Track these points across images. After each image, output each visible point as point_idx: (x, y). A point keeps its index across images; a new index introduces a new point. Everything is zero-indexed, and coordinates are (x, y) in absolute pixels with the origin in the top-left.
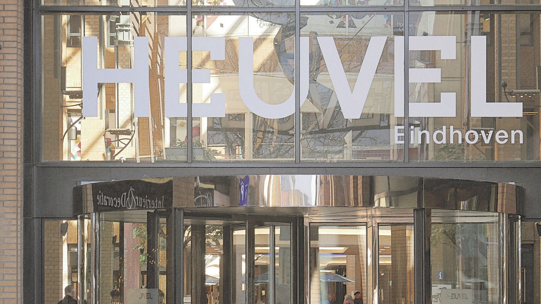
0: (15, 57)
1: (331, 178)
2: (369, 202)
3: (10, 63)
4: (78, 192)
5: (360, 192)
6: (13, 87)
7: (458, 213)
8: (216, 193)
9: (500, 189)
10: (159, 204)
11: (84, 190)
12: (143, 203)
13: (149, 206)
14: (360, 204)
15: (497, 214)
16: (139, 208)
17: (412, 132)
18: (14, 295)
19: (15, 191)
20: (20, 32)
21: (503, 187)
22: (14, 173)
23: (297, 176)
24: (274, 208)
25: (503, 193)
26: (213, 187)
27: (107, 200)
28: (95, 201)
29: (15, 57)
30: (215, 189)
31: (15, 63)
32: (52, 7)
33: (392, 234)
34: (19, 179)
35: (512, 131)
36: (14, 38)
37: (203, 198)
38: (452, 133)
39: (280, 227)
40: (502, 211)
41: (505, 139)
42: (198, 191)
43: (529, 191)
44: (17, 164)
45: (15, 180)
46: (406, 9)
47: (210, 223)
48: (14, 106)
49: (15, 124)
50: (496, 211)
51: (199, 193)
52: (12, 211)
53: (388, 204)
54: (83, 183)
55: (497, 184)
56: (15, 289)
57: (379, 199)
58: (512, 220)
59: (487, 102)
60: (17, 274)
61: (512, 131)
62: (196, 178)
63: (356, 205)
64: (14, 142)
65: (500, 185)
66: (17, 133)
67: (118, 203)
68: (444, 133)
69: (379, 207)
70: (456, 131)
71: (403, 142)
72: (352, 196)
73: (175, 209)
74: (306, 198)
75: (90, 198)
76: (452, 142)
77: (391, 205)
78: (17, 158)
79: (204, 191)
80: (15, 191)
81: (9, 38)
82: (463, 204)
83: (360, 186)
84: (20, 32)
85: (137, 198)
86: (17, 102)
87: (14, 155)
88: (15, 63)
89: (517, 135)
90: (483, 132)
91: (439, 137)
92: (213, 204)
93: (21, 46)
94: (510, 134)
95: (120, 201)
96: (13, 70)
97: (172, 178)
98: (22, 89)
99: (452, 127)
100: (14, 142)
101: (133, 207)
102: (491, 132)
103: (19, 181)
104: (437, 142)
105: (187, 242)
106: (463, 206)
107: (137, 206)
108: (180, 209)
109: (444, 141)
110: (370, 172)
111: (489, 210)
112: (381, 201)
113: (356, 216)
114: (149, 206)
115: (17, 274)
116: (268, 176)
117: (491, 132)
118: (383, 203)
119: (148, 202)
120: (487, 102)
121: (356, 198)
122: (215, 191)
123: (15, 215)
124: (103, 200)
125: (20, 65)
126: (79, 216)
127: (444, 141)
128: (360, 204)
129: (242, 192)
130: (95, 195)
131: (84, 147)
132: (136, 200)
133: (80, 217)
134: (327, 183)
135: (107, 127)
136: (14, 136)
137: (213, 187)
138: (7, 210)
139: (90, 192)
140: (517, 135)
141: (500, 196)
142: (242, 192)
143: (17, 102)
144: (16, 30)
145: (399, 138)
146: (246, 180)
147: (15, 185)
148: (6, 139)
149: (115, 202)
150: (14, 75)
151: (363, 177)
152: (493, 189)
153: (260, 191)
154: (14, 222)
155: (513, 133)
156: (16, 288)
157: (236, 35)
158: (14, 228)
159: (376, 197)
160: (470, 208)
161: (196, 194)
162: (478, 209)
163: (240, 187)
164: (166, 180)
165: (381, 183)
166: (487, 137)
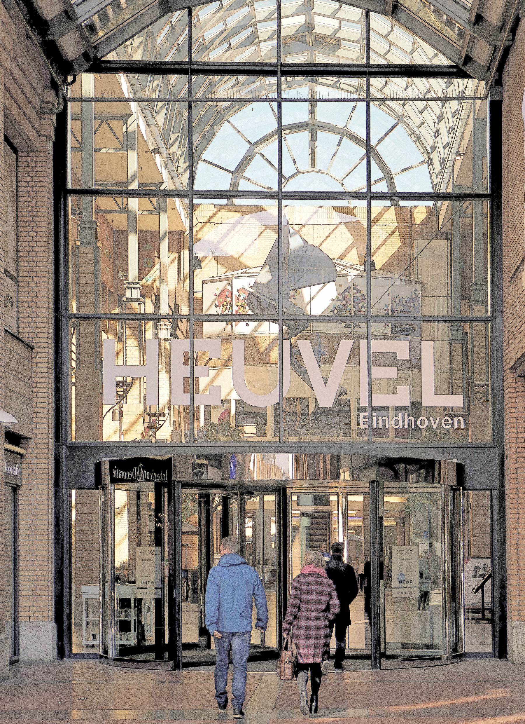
3: (42, 380)
4: (98, 466)
7: (408, 484)
10: (162, 477)
11: (103, 466)
12: (150, 476)
13: (154, 478)
19: (45, 466)
20: (50, 380)
24: (258, 480)
26: (207, 462)
28: (111, 474)
31: (46, 411)
32: (100, 190)
34: (50, 435)
35: (401, 427)
36: (46, 340)
37: (199, 471)
39: (64, 491)
41: (449, 424)
42: (195, 466)
45: (47, 472)
47: (213, 492)
49: (46, 411)
51: (196, 467)
53: (351, 477)
54: (103, 459)
57: (344, 472)
59: (436, 393)
61: (401, 427)
62: (193, 456)
63: (325, 478)
67: (130, 476)
70: (410, 418)
71: (367, 427)
72: (322, 470)
73: (174, 481)
74: (286, 472)
75: (108, 471)
76: (406, 426)
78: (48, 438)
80: (45, 466)
81: (41, 340)
82: (412, 477)
84: (50, 380)
85: (145, 472)
87: (46, 426)
88: (46, 360)
89: (459, 422)
92: (208, 477)
94: (453, 421)
95: (131, 474)
99: (406, 415)
101: (142, 479)
103: (50, 432)
104: (397, 427)
108: (178, 482)
109: (400, 426)
110: (336, 452)
112: (346, 475)
114: (154, 478)
116: (253, 454)
118: (348, 477)
119: (154, 476)
120: (436, 393)
121: (325, 472)
122: (209, 467)
123: (47, 460)
124: (118, 474)
127: (400, 426)
128: (328, 478)
129: (232, 466)
130: (111, 469)
133: (102, 487)
135: (145, 410)
137: (207, 462)
138: (40, 481)
139: (107, 467)
140: (459, 422)
142: (232, 466)
146: (233, 457)
148: (39, 423)
149: (127, 475)
150: (45, 400)
155: (456, 419)
158: (46, 497)
159: (341, 471)
160: (418, 481)
164: (167, 457)
165: (345, 460)
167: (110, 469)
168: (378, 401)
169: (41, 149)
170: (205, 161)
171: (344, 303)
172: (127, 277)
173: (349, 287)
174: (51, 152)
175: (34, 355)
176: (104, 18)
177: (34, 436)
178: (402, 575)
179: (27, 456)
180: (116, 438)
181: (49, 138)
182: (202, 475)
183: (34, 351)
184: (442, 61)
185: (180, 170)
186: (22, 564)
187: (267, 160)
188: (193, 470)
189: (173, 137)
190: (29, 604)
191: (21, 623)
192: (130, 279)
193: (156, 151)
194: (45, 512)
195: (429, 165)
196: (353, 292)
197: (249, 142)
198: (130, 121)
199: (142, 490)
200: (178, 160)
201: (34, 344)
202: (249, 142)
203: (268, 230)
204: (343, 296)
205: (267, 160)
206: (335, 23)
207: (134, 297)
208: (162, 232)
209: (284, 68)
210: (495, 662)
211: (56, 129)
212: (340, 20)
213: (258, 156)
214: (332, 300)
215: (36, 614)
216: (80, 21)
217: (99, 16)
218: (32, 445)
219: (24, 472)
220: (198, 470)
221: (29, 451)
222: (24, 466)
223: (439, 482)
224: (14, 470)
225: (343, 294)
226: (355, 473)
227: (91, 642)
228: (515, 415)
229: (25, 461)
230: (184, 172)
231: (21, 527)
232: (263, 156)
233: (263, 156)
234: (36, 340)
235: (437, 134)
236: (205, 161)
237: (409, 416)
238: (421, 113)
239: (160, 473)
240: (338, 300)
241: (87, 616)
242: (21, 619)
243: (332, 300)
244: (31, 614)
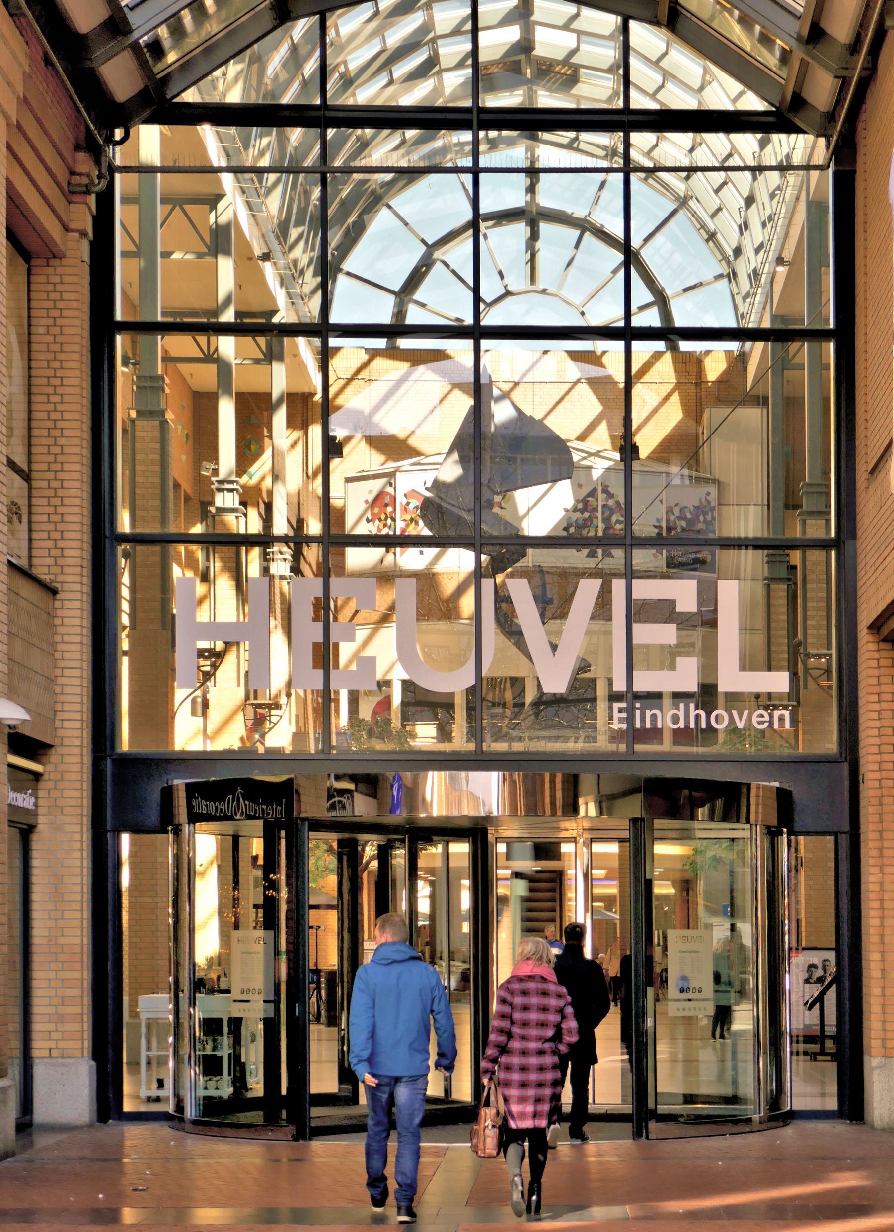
0: (78, 604)
1: (518, 776)
2: (572, 809)
5: (559, 794)
6: (77, 647)
8: (357, 796)
9: (753, 792)
10: (277, 811)
11: (175, 792)
12: (256, 810)
14: (559, 813)
15: (749, 826)
16: (249, 817)
17: (638, 712)
18: (77, 940)
20: (85, 518)
21: (758, 787)
22: (78, 733)
23: (472, 774)
24: (438, 819)
25: (758, 796)
26: (352, 786)
27: (206, 806)
28: (190, 807)
29: (78, 690)
30: (356, 790)
33: (620, 851)
37: (340, 802)
38: (693, 713)
40: (757, 821)
42: (332, 793)
43: (799, 795)
44: (82, 755)
46: (628, 542)
47: (362, 837)
48: (77, 673)
50: (748, 821)
52: (75, 822)
54: (176, 782)
55: (749, 786)
56: (79, 932)
57: (586, 804)
58: (773, 833)
59: (743, 668)
60: (82, 901)
62: (329, 775)
63: (554, 813)
64: (78, 725)
65: (753, 786)
66: (82, 720)
67: (221, 810)
68: (681, 714)
69: (586, 816)
76: (692, 726)
77: (601, 813)
79: (342, 792)
81: (70, 578)
83: (559, 786)
85: (247, 803)
86: (82, 686)
89: (781, 719)
90: (734, 712)
91: (676, 719)
92: (353, 812)
93: (87, 589)
95: (223, 807)
96: (75, 666)
97: (292, 776)
98: (90, 599)
99: (692, 706)
100: (78, 699)
101: (242, 815)
102: (746, 713)
104: (676, 727)
105: (368, 863)
106: (703, 815)
107: (247, 815)
111: (738, 821)
112: (588, 808)
113: (559, 829)
114: (263, 814)
115: (82, 910)
117: (746, 713)
118: (592, 811)
119: (263, 810)
124: (202, 806)
125: (85, 547)
126: (170, 828)
127: (681, 725)
128: (559, 813)
129: (395, 793)
131: (211, 727)
132: (246, 805)
134: (513, 783)
135: (247, 697)
136: (77, 510)
137: (352, 786)
140: (781, 719)
141: (753, 801)
142: (395, 793)
143: (81, 643)
144: (80, 568)
145: (620, 720)
147: (78, 785)
149: (216, 808)
151: (563, 775)
152: (744, 790)
153: (420, 792)
154: (78, 837)
156: (80, 878)
157: (437, 568)
158: (77, 845)
159: (581, 801)
160: (711, 818)
161: (330, 797)
162: (725, 819)
163: (392, 786)
164: (283, 778)
165: (587, 781)
166: (740, 719)
167: (187, 798)
168: (644, 682)
169: (69, 253)
170: (349, 274)
171: (586, 515)
172: (216, 472)
173: (594, 490)
174: (87, 257)
175: (58, 604)
176: (178, 31)
177: (57, 742)
178: (684, 978)
179: (46, 777)
180: (196, 745)
181: (83, 234)
182: (344, 808)
183: (58, 597)
184: (753, 103)
185: (307, 289)
186: (37, 960)
187: (454, 272)
188: (328, 800)
189: (294, 233)
190: (51, 1027)
191: (36, 1061)
192: (222, 475)
193: (266, 257)
194: (78, 871)
195: (730, 281)
196: (601, 496)
197: (423, 241)
198: (221, 206)
199: (240, 834)
200: (302, 273)
201: (58, 586)
202: (423, 241)
203: (457, 393)
204: (584, 504)
205: (454, 272)
206: (568, 40)
207: (229, 505)
208: (275, 395)
209: (483, 116)
210: (841, 1128)
211: (95, 218)
212: (579, 33)
213: (438, 266)
214: (567, 511)
215: (61, 1044)
216: (135, 35)
217: (168, 27)
218: (54, 756)
219: (41, 802)
220: (336, 799)
221: (50, 767)
222: (41, 793)
223: (748, 821)
224: (25, 801)
225: (585, 501)
226: (604, 805)
227: (155, 1092)
228: (876, 707)
229: (42, 784)
230: (314, 292)
231: (36, 896)
232: (446, 265)
233: (446, 265)
234: (60, 578)
235: (744, 227)
236: (349, 274)
237: (697, 708)
238: (717, 191)
239: (272, 806)
240: (575, 510)
241: (149, 1048)
242: (35, 1053)
243: (567, 511)
244: (52, 1044)
